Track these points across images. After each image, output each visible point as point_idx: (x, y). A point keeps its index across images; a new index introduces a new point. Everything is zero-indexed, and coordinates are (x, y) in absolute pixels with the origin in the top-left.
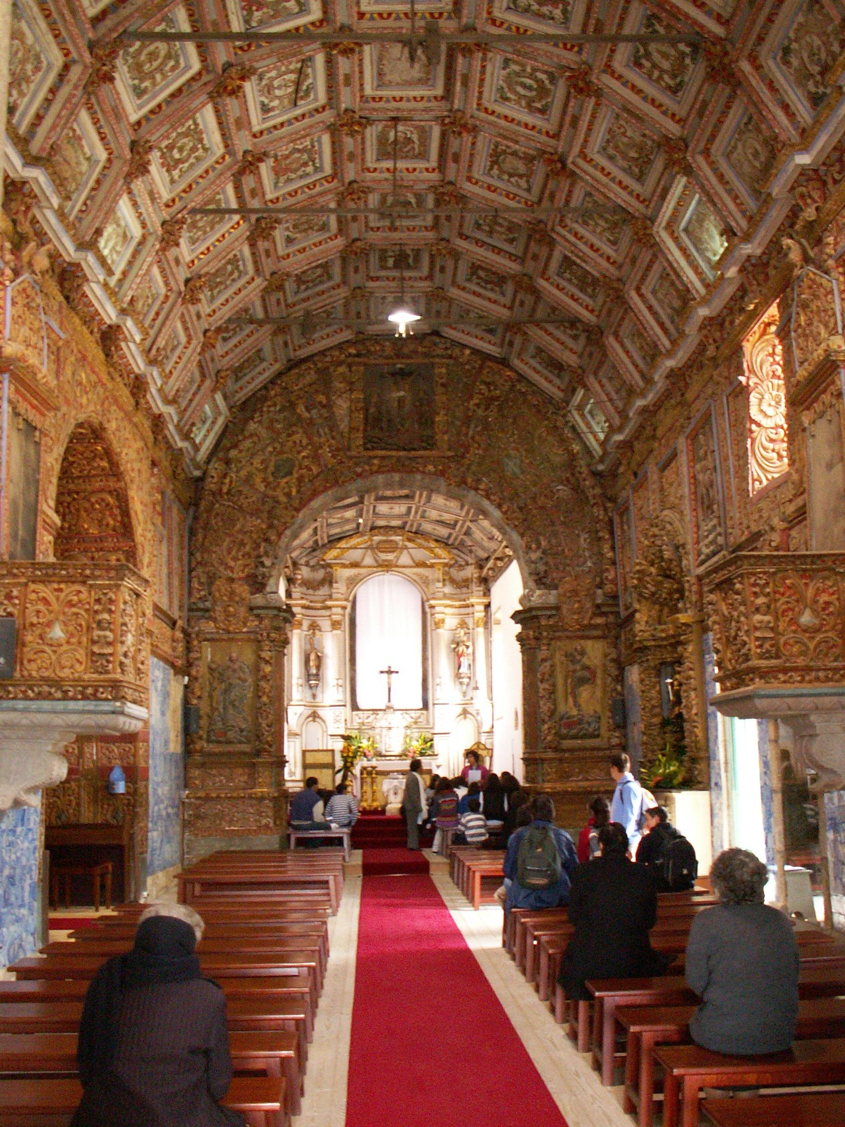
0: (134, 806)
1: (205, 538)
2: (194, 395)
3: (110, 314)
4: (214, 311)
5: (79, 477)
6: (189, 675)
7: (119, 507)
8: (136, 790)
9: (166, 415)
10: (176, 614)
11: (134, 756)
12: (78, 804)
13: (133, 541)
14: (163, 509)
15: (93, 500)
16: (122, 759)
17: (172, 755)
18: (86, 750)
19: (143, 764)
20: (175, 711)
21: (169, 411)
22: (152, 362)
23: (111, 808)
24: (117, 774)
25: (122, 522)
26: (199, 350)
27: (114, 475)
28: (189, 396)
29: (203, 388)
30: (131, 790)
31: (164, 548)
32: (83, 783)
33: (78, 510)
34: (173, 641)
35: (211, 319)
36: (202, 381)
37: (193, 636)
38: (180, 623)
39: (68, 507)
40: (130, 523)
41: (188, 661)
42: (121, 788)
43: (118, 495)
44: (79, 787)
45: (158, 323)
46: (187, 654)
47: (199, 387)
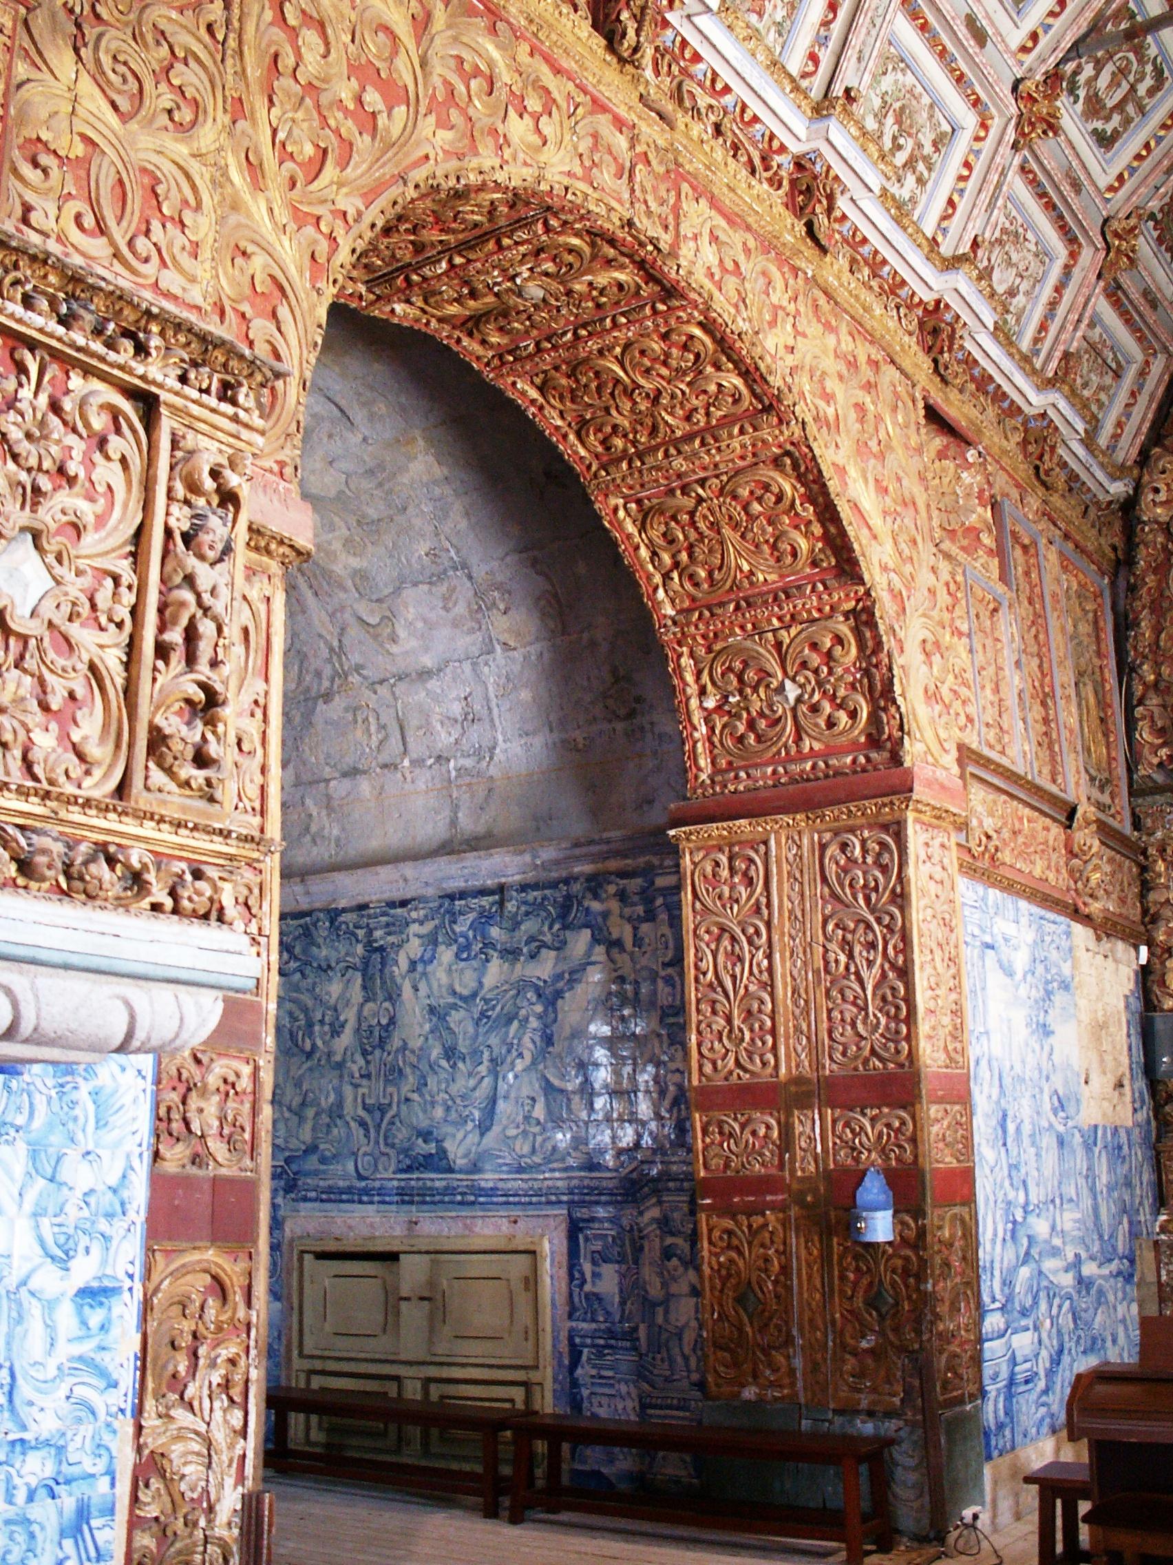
0: (920, 1277)
1: (1158, 630)
2: (1058, 290)
3: (794, 129)
4: (1034, 37)
5: (688, 438)
6: (1150, 944)
7: (809, 498)
8: (922, 1233)
9: (949, 298)
10: (1075, 786)
11: (913, 1140)
12: (785, 1270)
13: (862, 582)
14: (999, 540)
15: (744, 493)
16: (883, 1152)
17: (1090, 1138)
18: (798, 1128)
19: (947, 1160)
20: (1099, 1028)
21: (955, 290)
22: (821, 109)
23: (865, 1281)
24: (873, 1189)
25: (826, 537)
26: (1011, 135)
27: (768, 409)
28: (1047, 292)
29: (1077, 273)
30: (911, 1234)
31: (1009, 627)
32: (794, 1212)
33: (715, 526)
34: (1072, 854)
35: (1028, 59)
36: (1073, 255)
37: (1152, 851)
38: (1085, 810)
39: (693, 523)
40: (843, 533)
41: (1145, 911)
42: (880, 1227)
43: (795, 466)
44: (785, 1223)
45: (837, 27)
46: (1142, 896)
47: (1067, 270)
